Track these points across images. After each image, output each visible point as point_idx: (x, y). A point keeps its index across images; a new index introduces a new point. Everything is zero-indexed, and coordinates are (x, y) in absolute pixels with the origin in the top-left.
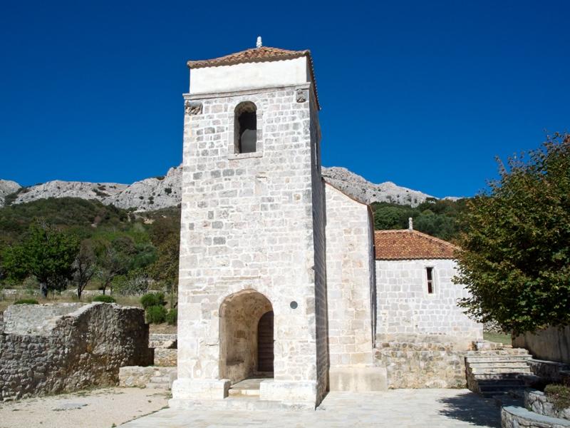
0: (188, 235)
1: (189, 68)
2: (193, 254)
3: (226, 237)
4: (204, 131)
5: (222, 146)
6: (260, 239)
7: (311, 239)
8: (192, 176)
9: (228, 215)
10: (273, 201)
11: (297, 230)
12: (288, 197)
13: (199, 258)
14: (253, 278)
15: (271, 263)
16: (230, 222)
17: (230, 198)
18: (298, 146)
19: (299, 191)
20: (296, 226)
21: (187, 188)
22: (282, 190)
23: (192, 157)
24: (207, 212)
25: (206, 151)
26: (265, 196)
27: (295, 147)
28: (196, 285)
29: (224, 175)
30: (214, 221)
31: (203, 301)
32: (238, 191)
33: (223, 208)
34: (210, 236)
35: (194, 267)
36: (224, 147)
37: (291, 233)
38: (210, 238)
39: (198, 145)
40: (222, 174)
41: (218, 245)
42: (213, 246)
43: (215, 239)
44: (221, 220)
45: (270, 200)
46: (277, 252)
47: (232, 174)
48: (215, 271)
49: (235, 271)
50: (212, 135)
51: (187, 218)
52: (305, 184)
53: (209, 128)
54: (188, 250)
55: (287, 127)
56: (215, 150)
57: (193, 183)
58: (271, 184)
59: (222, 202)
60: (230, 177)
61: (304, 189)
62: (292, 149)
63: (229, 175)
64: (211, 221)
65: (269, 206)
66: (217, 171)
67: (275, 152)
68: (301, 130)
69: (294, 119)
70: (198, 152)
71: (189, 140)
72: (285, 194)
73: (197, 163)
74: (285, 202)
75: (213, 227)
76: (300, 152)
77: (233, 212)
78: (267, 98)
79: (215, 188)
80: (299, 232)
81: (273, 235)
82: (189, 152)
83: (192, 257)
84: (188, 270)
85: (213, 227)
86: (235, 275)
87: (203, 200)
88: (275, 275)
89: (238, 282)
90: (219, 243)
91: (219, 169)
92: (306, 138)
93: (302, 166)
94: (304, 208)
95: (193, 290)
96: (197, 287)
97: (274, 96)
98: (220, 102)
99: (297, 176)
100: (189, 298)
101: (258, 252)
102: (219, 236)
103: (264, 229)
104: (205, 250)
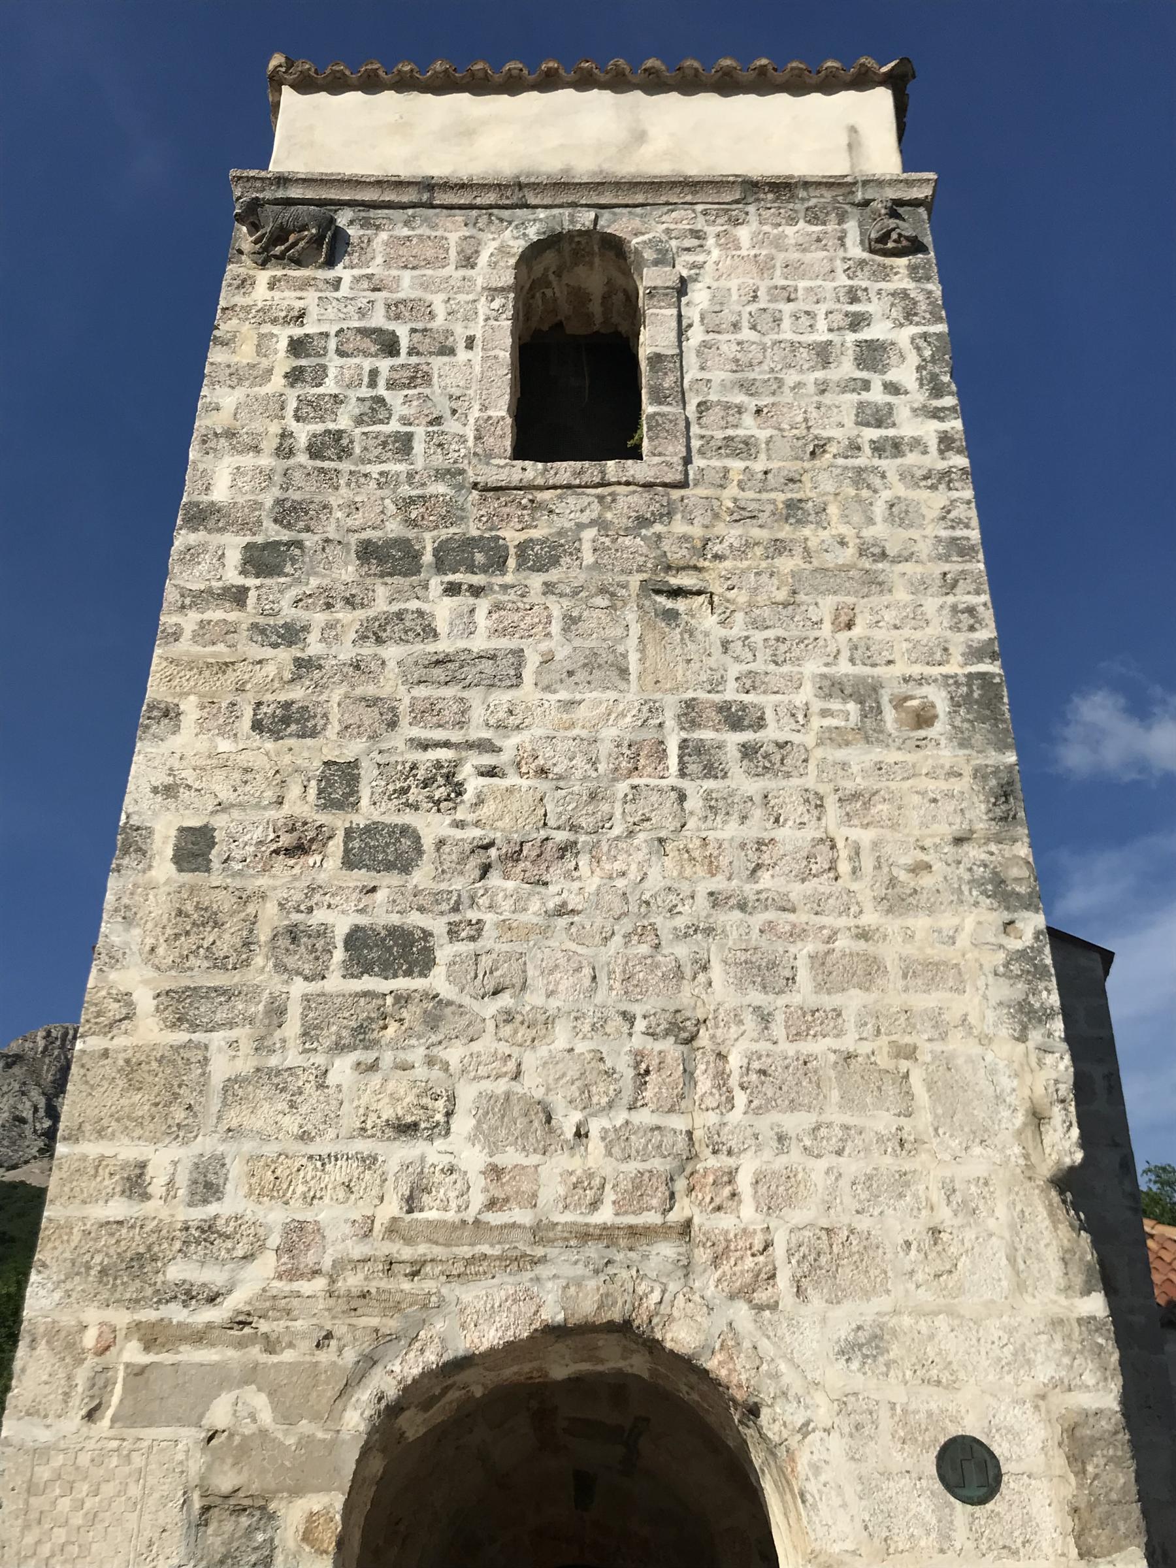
0: (158, 907)
1: (276, 82)
2: (181, 1037)
3: (437, 925)
4: (332, 344)
5: (437, 421)
6: (682, 951)
7: (1040, 972)
8: (234, 557)
9: (459, 790)
10: (760, 723)
11: (931, 911)
12: (852, 707)
13: (221, 1068)
14: (633, 1232)
15: (764, 1124)
16: (474, 833)
17: (474, 696)
18: (896, 447)
19: (921, 681)
20: (927, 881)
21: (189, 621)
22: (812, 667)
23: (248, 460)
24: (316, 766)
25: (291, 453)
26: (702, 695)
27: (878, 448)
28: (176, 1272)
29: (440, 566)
30: (360, 821)
31: (220, 1414)
32: (532, 660)
33: (425, 746)
34: (320, 916)
35: (180, 1133)
36: (452, 426)
37: (893, 925)
38: (324, 931)
39: (292, 405)
40: (428, 558)
41: (369, 983)
42: (335, 983)
43: (356, 940)
44: (408, 818)
45: (734, 717)
46: (808, 1047)
47: (498, 563)
48: (337, 1173)
49: (495, 1172)
50: (384, 365)
51: (169, 791)
52: (959, 642)
53: (364, 332)
54: (145, 1001)
55: (824, 354)
56: (397, 436)
57: (238, 596)
58: (738, 628)
59: (426, 712)
60: (478, 579)
61: (955, 667)
62: (861, 461)
63: (471, 569)
64: (339, 821)
65: (732, 753)
66: (403, 544)
67: (759, 466)
68: (905, 373)
69: (857, 322)
70: (285, 435)
71: (236, 377)
72: (832, 688)
73: (276, 492)
74: (834, 737)
75: (349, 862)
76: (905, 475)
77: (491, 772)
78: (700, 224)
79: (375, 633)
80: (947, 921)
81: (768, 928)
82: (230, 434)
83: (173, 1058)
84: (127, 1151)
85: (349, 862)
86: (492, 1204)
87: (297, 693)
88: (798, 1216)
89: (518, 1261)
90: (387, 970)
91: (411, 534)
92: (937, 414)
93: (924, 548)
94: (967, 779)
95: (149, 1315)
96: (188, 1295)
97: (736, 222)
98: (407, 223)
99: (902, 595)
100: (100, 1384)
101: (668, 1045)
102: (395, 919)
103: (702, 889)
104: (277, 1012)
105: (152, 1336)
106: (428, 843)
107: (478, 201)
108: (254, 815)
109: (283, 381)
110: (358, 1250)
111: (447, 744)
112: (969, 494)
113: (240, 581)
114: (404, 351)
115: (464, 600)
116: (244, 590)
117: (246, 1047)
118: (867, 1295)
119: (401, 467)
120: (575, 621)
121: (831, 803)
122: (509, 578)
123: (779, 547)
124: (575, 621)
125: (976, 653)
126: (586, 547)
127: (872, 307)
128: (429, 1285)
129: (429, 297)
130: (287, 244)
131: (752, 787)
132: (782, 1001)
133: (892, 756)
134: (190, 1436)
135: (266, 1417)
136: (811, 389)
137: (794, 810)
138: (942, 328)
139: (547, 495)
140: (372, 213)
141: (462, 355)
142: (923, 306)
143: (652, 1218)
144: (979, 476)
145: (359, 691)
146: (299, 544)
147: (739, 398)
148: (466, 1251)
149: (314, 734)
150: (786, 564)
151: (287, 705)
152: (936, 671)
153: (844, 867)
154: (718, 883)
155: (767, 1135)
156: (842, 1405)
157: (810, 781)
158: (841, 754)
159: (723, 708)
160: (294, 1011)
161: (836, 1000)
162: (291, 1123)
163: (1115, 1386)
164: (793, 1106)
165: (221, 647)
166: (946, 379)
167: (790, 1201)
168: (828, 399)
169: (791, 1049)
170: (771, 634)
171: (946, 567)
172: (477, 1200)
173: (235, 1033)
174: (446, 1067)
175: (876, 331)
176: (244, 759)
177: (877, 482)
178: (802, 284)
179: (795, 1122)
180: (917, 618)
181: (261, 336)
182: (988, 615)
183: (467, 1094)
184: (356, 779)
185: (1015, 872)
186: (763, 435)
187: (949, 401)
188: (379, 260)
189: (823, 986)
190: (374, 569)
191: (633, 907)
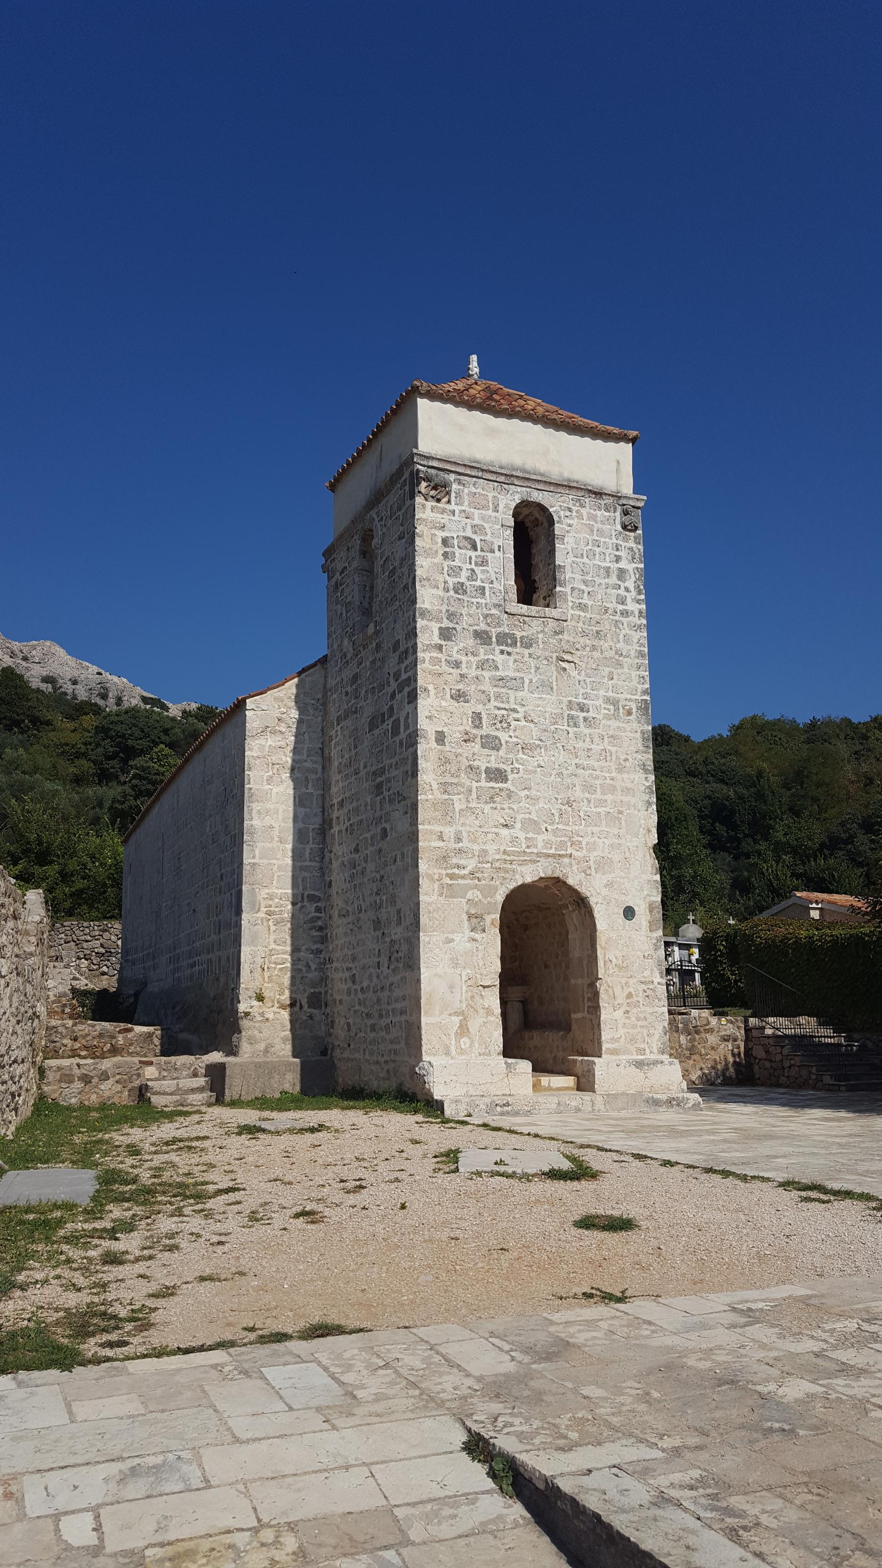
2: (446, 797)
7: (652, 792)
12: (612, 707)
13: (458, 806)
14: (559, 855)
15: (589, 829)
19: (630, 700)
20: (628, 764)
22: (602, 693)
25: (448, 591)
26: (574, 699)
28: (455, 861)
29: (499, 643)
31: (470, 895)
32: (527, 681)
33: (499, 709)
37: (619, 776)
40: (494, 639)
42: (483, 783)
45: (582, 708)
48: (490, 836)
60: (509, 649)
62: (617, 618)
66: (486, 632)
68: (630, 584)
69: (618, 559)
72: (608, 700)
74: (607, 717)
79: (481, 666)
80: (632, 776)
81: (590, 775)
84: (437, 828)
86: (528, 847)
90: (496, 780)
91: (488, 629)
94: (639, 733)
96: (459, 867)
102: (497, 766)
105: (452, 877)
106: (503, 742)
107: (498, 479)
108: (455, 728)
109: (442, 558)
110: (497, 857)
111: (505, 709)
112: (645, 634)
113: (439, 642)
114: (479, 549)
115: (505, 656)
116: (441, 646)
117: (464, 800)
118: (610, 873)
119: (483, 601)
120: (538, 668)
121: (606, 738)
122: (518, 650)
123: (594, 648)
124: (538, 668)
125: (645, 692)
126: (540, 641)
127: (622, 553)
128: (514, 867)
129: (485, 525)
130: (537, 496)
131: (587, 731)
132: (593, 796)
133: (621, 725)
134: (464, 901)
135: (480, 897)
136: (604, 586)
137: (596, 740)
138: (642, 566)
139: (526, 619)
140: (461, 477)
141: (497, 553)
142: (637, 556)
143: (564, 852)
144: (649, 627)
145: (478, 688)
146: (455, 629)
147: (583, 587)
148: (522, 858)
149: (468, 702)
150: (597, 654)
151: (459, 691)
152: (634, 697)
153: (608, 758)
154: (577, 761)
155: (589, 832)
156: (604, 898)
157: (600, 731)
158: (609, 723)
159: (579, 704)
160: (474, 791)
161: (606, 797)
162: (477, 823)
163: (660, 896)
164: (596, 825)
165: (437, 667)
166: (642, 587)
167: (594, 849)
168: (608, 591)
169: (594, 810)
170: (591, 679)
171: (638, 661)
172: (524, 846)
173: (460, 796)
174: (513, 810)
175: (623, 565)
176: (451, 709)
177: (621, 626)
178: (603, 540)
179: (596, 829)
180: (629, 678)
181: (432, 534)
182: (647, 679)
183: (520, 817)
184: (481, 718)
185: (648, 763)
186: (590, 603)
187: (643, 597)
188: (466, 503)
189: (603, 794)
190: (479, 642)
191: (556, 767)
